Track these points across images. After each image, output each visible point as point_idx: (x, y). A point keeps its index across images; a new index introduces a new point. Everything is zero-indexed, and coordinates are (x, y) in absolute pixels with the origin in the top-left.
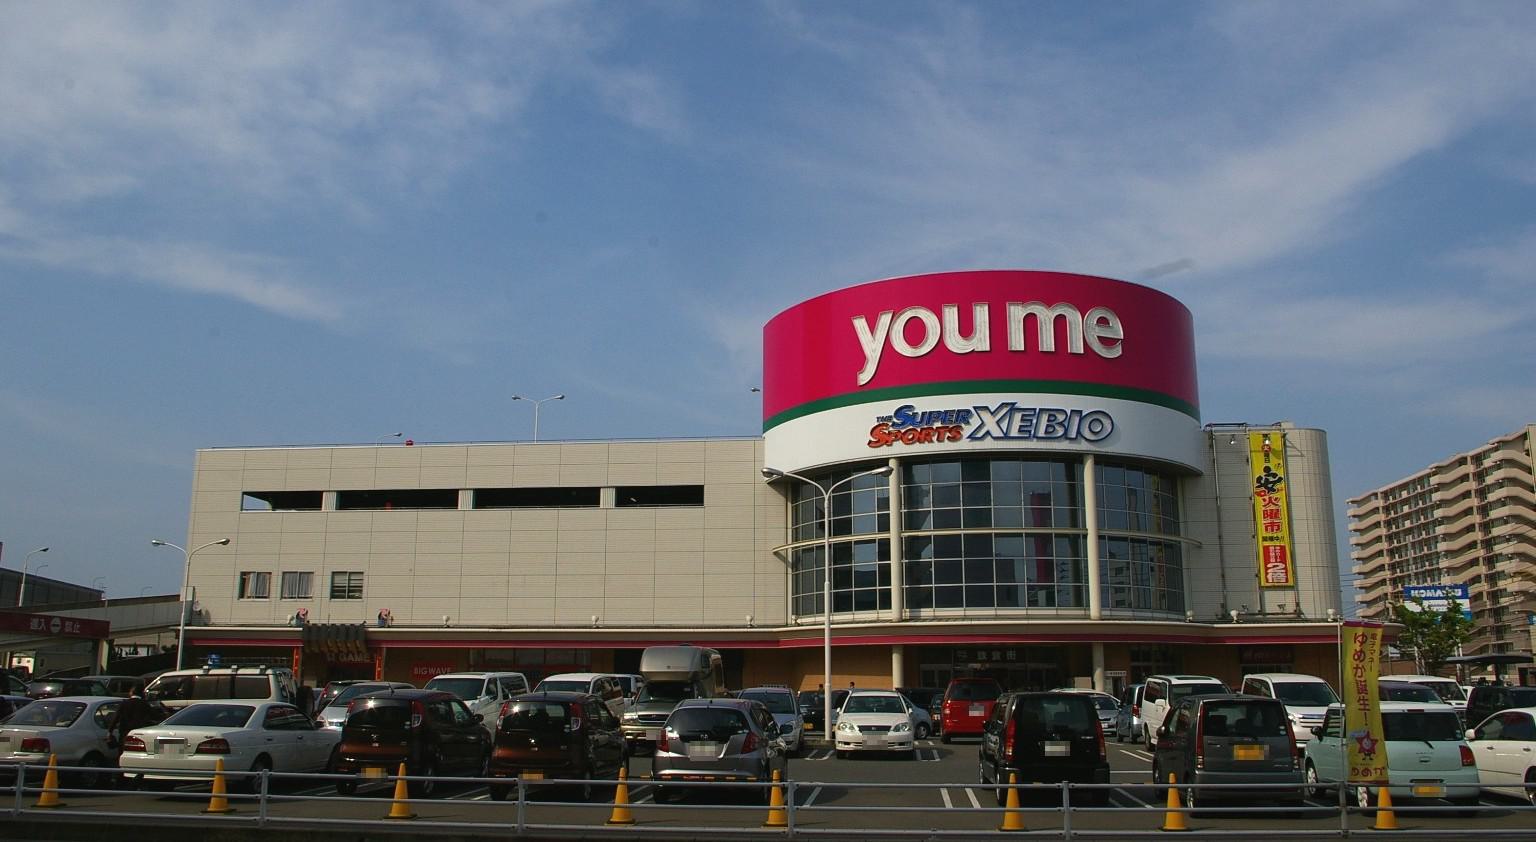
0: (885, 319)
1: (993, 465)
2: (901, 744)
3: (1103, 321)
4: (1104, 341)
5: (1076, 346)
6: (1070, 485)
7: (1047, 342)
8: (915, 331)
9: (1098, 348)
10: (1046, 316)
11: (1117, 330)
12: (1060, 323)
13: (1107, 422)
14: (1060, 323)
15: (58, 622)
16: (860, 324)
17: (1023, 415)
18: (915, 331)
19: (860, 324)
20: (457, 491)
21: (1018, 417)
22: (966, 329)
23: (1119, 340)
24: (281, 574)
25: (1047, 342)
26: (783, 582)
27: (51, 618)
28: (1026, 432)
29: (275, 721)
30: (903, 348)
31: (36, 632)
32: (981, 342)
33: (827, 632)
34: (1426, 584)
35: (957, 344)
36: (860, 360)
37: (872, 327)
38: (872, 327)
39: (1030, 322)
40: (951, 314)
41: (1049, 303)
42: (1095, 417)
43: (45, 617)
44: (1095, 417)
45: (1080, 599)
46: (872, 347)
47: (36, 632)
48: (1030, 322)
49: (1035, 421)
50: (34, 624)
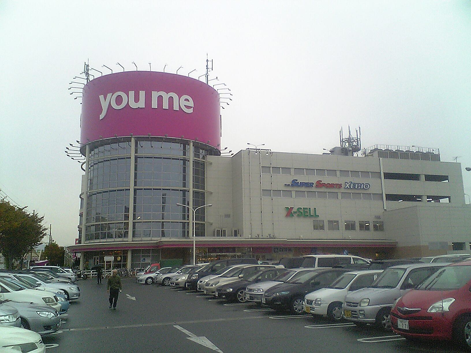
0: (109, 95)
3: (187, 100)
6: (137, 171)
7: (166, 106)
8: (119, 100)
10: (166, 97)
11: (191, 103)
13: (369, 186)
16: (101, 97)
18: (119, 100)
19: (101, 97)
20: (420, 175)
22: (137, 100)
23: (192, 107)
25: (166, 106)
29: (224, 231)
32: (142, 104)
33: (194, 242)
34: (308, 212)
35: (133, 105)
39: (160, 98)
40: (132, 93)
42: (366, 184)
44: (366, 184)
45: (400, 153)
48: (160, 98)
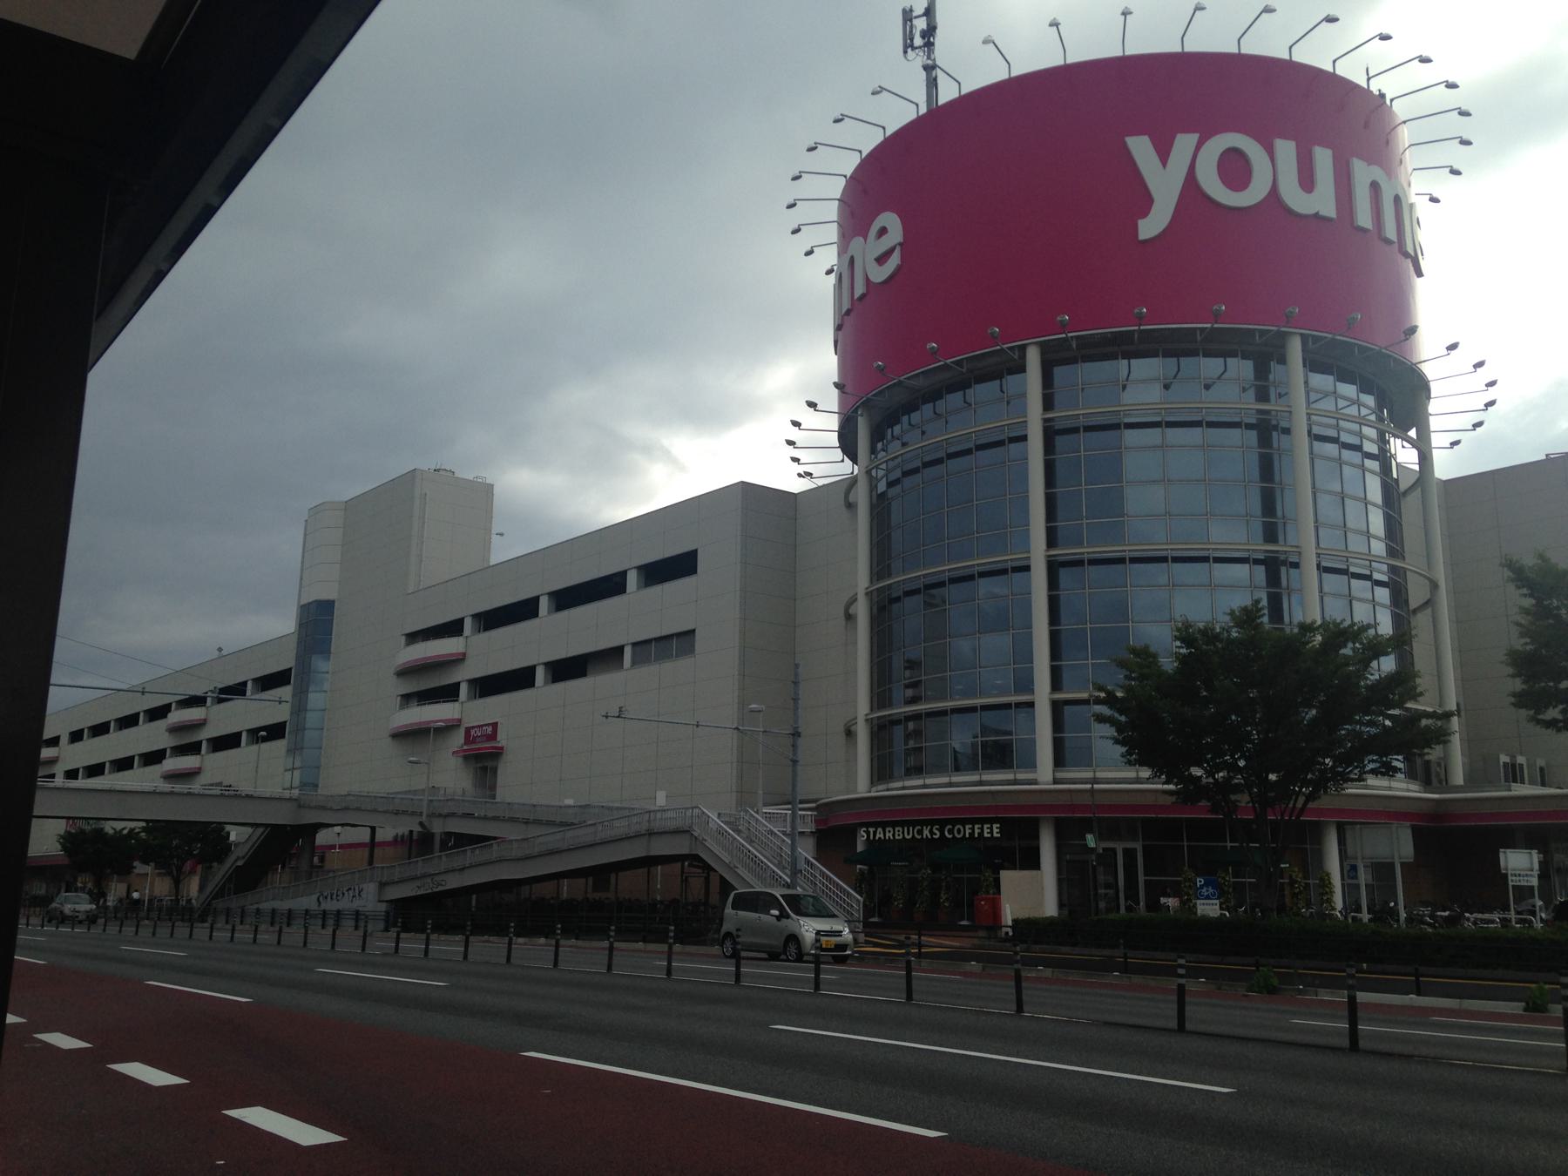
0: (1184, 143)
18: (1235, 169)
19: (1140, 148)
22: (1307, 181)
36: (1144, 202)
37: (1164, 158)
38: (1164, 158)
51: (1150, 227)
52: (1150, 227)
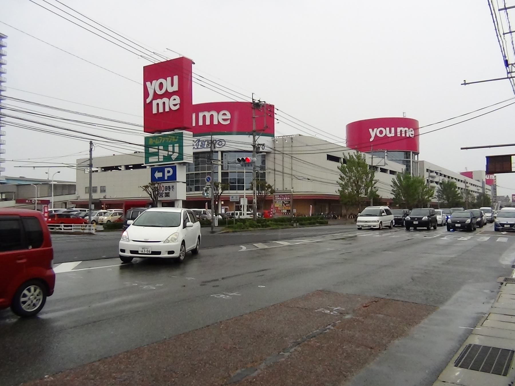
0: (375, 129)
1: (512, 156)
2: (373, 226)
4: (224, 120)
5: (408, 136)
8: (381, 132)
9: (411, 136)
10: (208, 115)
12: (212, 116)
14: (212, 116)
15: (34, 201)
17: (201, 142)
18: (381, 132)
19: (370, 130)
21: (200, 143)
24: (100, 187)
25: (208, 122)
26: (87, 198)
27: (32, 200)
28: (202, 146)
30: (378, 135)
31: (27, 203)
40: (388, 129)
41: (209, 111)
43: (30, 200)
46: (373, 135)
47: (27, 203)
48: (204, 117)
49: (204, 144)
50: (27, 201)
51: (371, 140)
52: (371, 140)
